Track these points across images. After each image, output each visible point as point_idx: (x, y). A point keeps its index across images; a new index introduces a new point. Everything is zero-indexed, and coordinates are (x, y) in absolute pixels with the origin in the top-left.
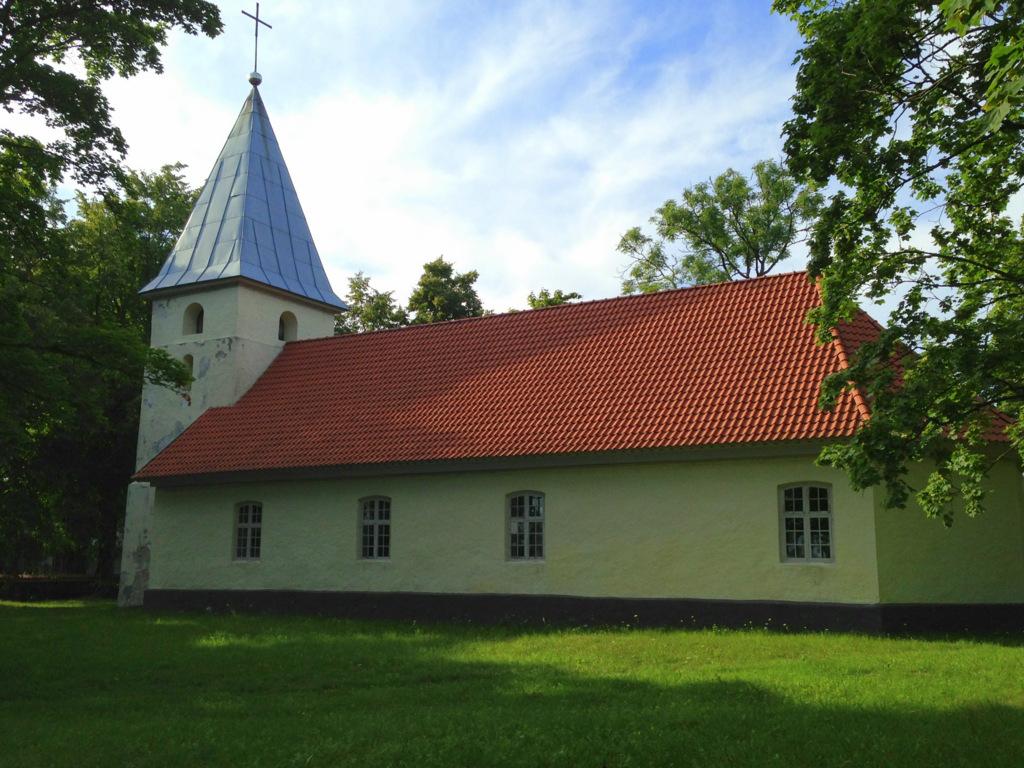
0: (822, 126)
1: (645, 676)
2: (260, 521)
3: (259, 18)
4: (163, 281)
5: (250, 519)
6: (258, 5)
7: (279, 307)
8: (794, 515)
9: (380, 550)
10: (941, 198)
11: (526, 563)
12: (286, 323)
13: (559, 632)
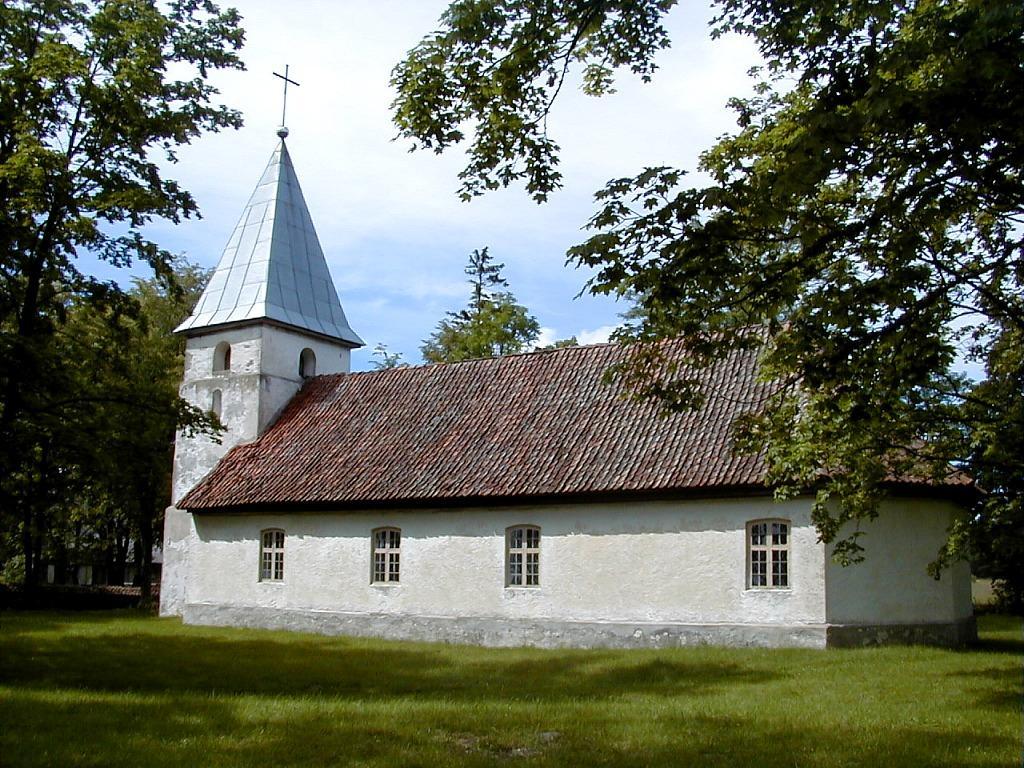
4: (200, 318)
9: (529, 578)
11: (271, 582)
12: (306, 357)
13: (427, 656)
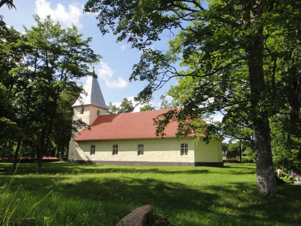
0: (4, 97)
1: (176, 181)
2: (95, 148)
5: (115, 147)
7: (97, 109)
8: (183, 148)
10: (69, 101)
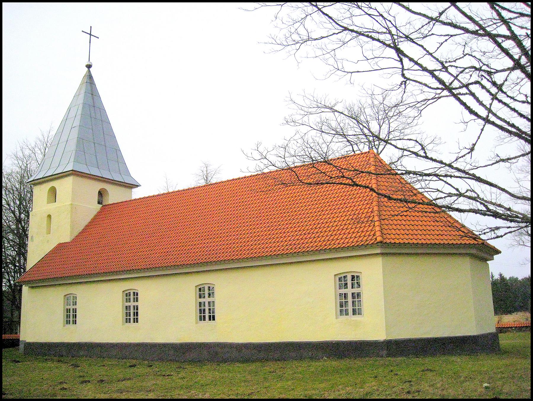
3: (91, 34)
6: (91, 27)
7: (100, 186)
